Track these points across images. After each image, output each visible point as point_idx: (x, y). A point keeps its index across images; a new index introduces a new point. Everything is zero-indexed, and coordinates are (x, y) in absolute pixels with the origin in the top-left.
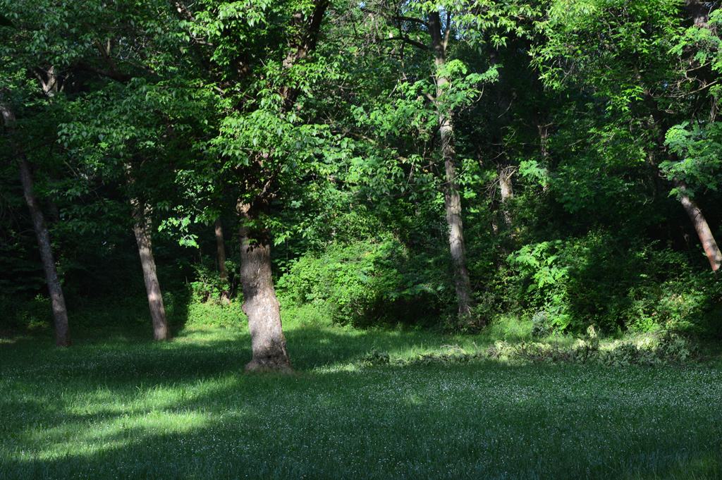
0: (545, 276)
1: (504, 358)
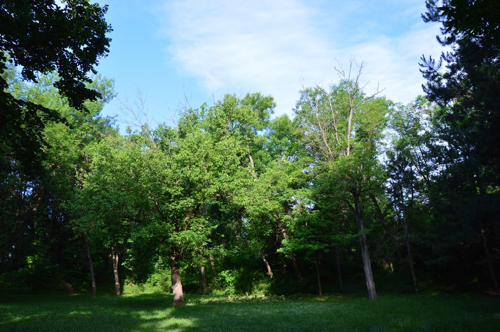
0: (229, 279)
1: (231, 301)
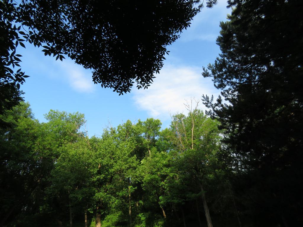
0: (143, 218)
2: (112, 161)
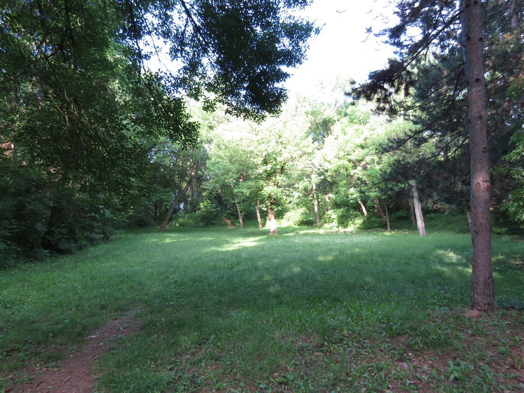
2: (280, 147)
